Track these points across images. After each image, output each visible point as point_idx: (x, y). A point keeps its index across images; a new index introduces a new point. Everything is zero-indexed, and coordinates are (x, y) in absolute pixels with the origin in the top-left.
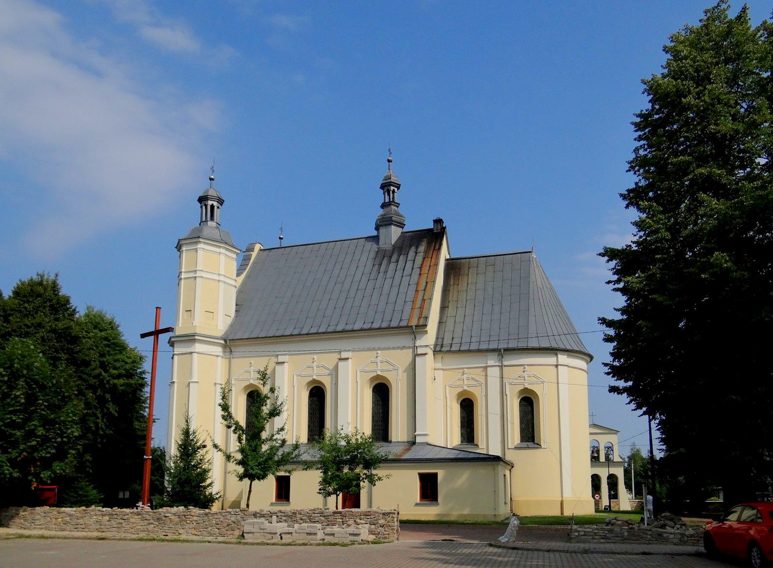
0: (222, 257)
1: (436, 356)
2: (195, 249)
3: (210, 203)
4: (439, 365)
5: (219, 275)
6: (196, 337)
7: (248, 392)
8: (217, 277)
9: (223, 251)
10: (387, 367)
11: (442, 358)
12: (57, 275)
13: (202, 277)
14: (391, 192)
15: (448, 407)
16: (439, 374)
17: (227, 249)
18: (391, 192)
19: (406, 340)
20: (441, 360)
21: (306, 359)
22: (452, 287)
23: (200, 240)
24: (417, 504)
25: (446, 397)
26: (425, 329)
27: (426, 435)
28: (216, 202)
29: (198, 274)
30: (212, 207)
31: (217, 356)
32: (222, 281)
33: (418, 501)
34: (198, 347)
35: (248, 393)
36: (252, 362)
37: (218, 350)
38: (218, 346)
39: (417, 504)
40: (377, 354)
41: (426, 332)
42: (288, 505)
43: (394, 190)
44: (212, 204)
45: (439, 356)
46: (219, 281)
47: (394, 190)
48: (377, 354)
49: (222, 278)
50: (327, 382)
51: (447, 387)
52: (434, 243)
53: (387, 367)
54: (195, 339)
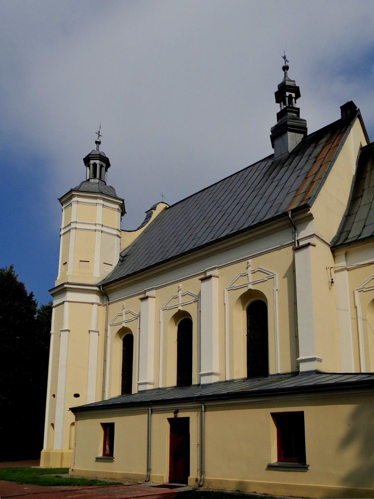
0: (100, 208)
1: (336, 254)
2: (204, 272)
3: (92, 162)
4: (342, 263)
5: (95, 224)
6: (66, 286)
7: (123, 338)
8: (93, 227)
9: (101, 201)
10: (260, 276)
11: (346, 254)
12: (11, 267)
13: (76, 228)
14: (287, 98)
15: (359, 319)
16: (342, 279)
17: (104, 200)
18: (287, 98)
19: (285, 238)
20: (344, 258)
21: (171, 290)
22: (368, 174)
23: (73, 193)
24: (271, 467)
25: (356, 307)
26: (309, 212)
27: (314, 359)
28: (98, 161)
29: (73, 225)
30: (95, 165)
31: (92, 304)
32: (98, 230)
33: (274, 460)
34: (69, 296)
35: (123, 338)
36: (124, 304)
37: (95, 298)
38: (93, 293)
39: (271, 467)
40: (248, 263)
41: (311, 217)
42: (305, 472)
43: (290, 95)
44: (95, 163)
45: (341, 254)
46: (95, 230)
47: (290, 95)
48: (248, 263)
49: (99, 228)
50: (191, 310)
51: (356, 292)
52: (340, 130)
53: (260, 276)
54: (65, 288)
